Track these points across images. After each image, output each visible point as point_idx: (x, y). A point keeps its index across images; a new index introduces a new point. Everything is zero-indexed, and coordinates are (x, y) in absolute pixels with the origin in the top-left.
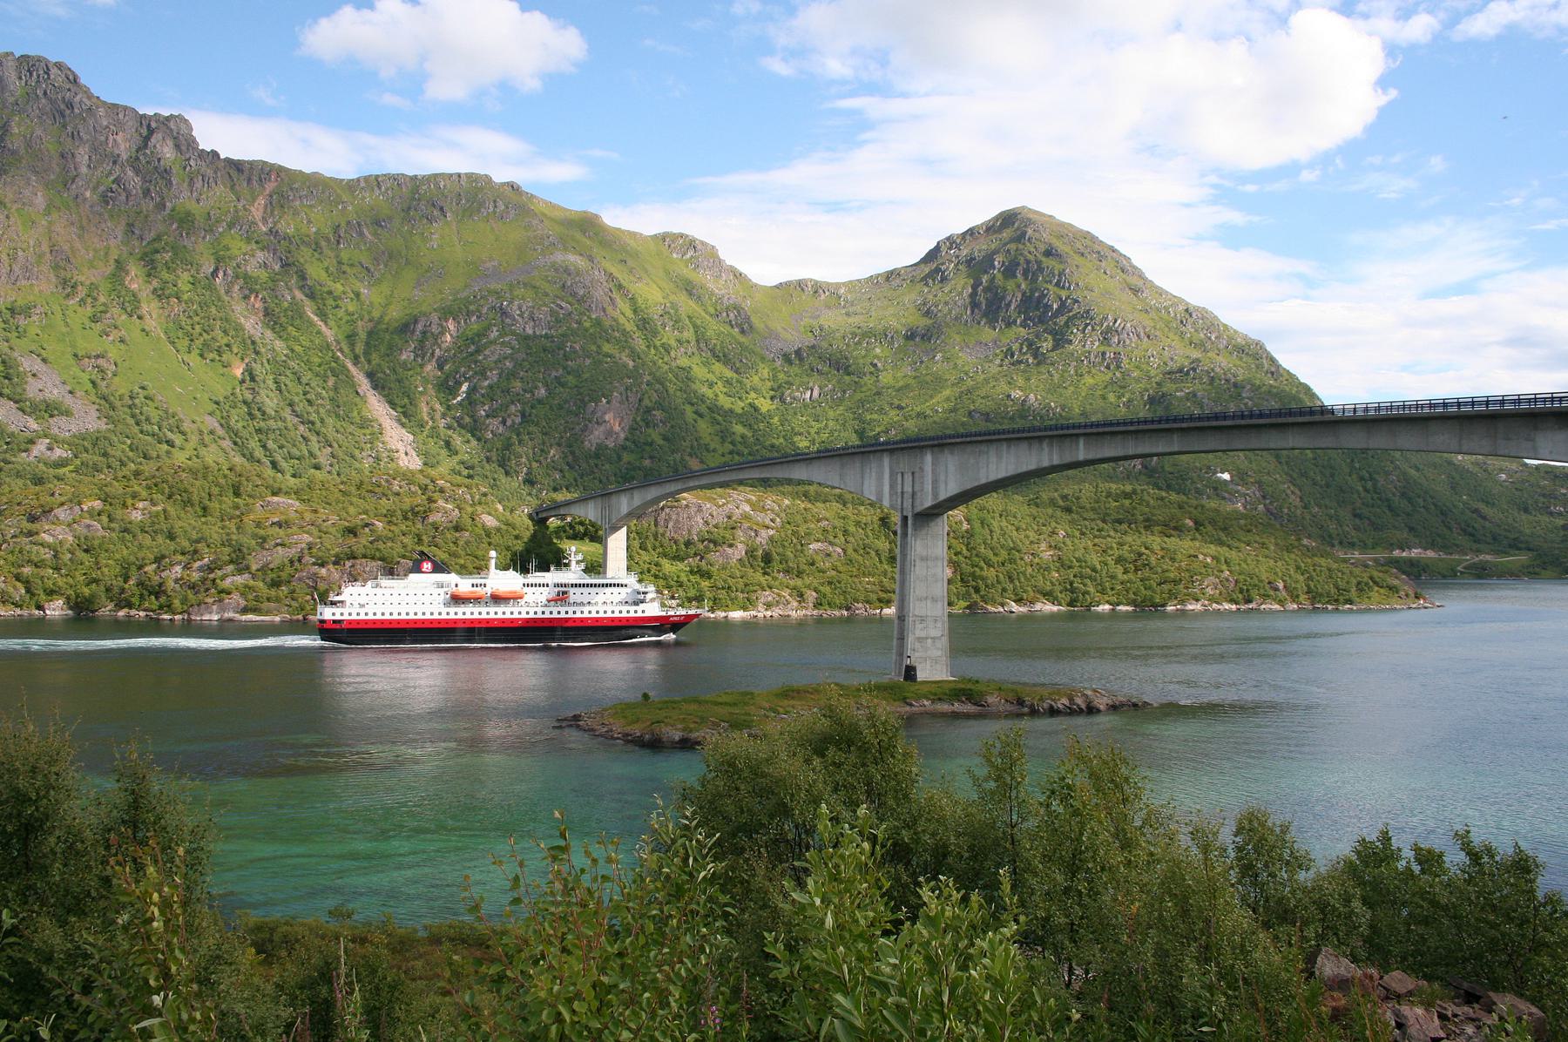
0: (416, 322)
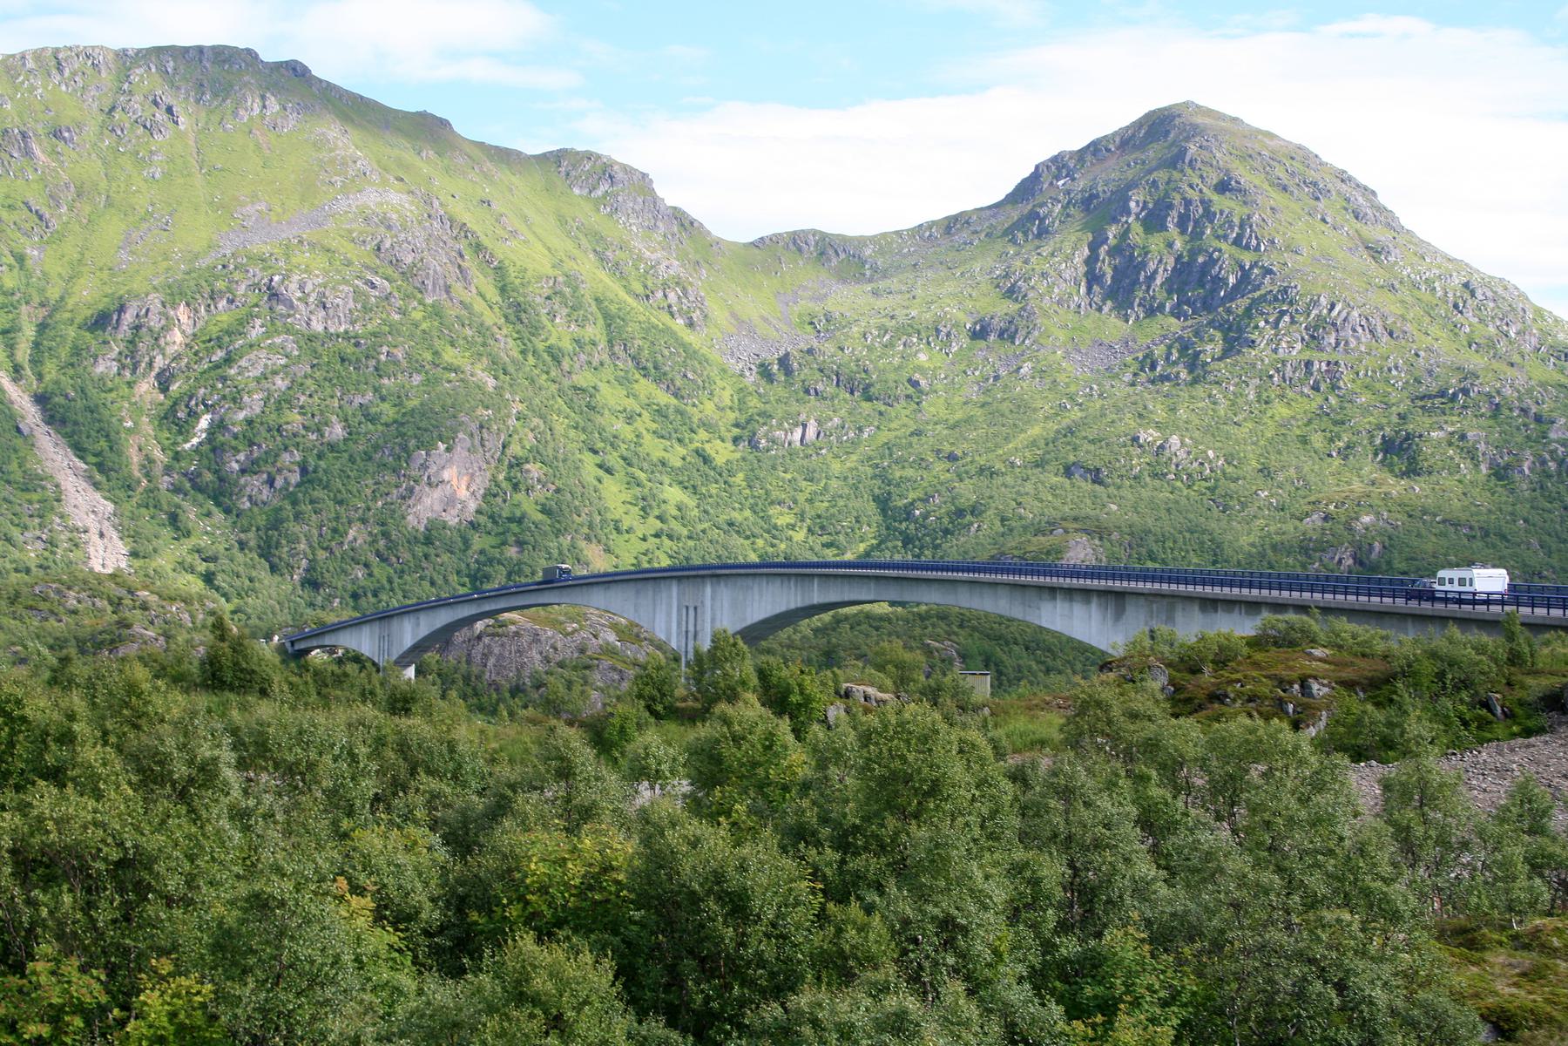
0: (122, 309)
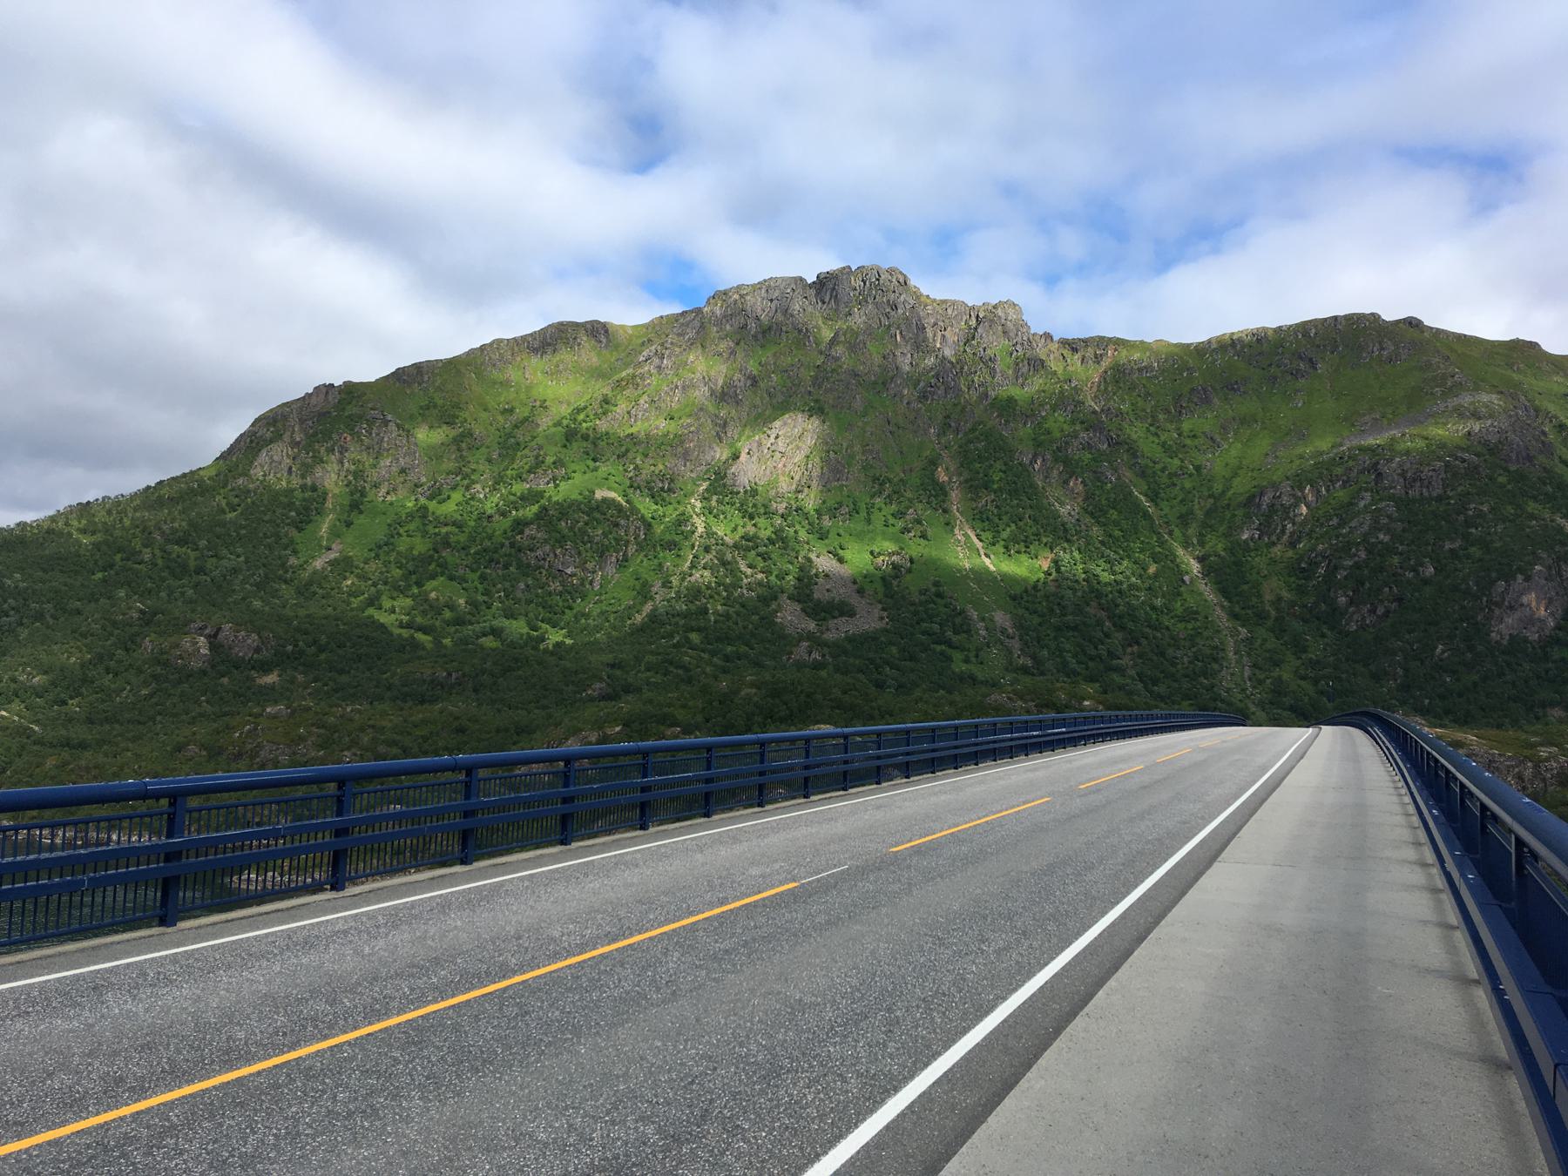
0: (1262, 494)
